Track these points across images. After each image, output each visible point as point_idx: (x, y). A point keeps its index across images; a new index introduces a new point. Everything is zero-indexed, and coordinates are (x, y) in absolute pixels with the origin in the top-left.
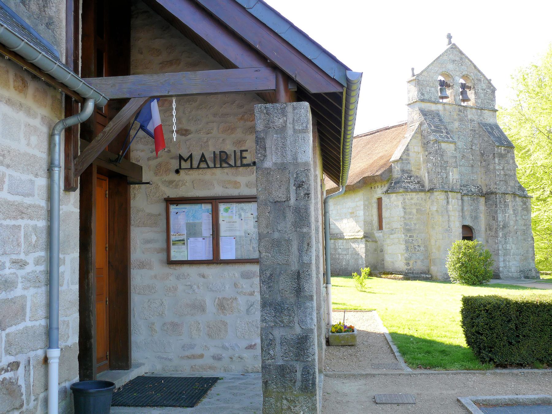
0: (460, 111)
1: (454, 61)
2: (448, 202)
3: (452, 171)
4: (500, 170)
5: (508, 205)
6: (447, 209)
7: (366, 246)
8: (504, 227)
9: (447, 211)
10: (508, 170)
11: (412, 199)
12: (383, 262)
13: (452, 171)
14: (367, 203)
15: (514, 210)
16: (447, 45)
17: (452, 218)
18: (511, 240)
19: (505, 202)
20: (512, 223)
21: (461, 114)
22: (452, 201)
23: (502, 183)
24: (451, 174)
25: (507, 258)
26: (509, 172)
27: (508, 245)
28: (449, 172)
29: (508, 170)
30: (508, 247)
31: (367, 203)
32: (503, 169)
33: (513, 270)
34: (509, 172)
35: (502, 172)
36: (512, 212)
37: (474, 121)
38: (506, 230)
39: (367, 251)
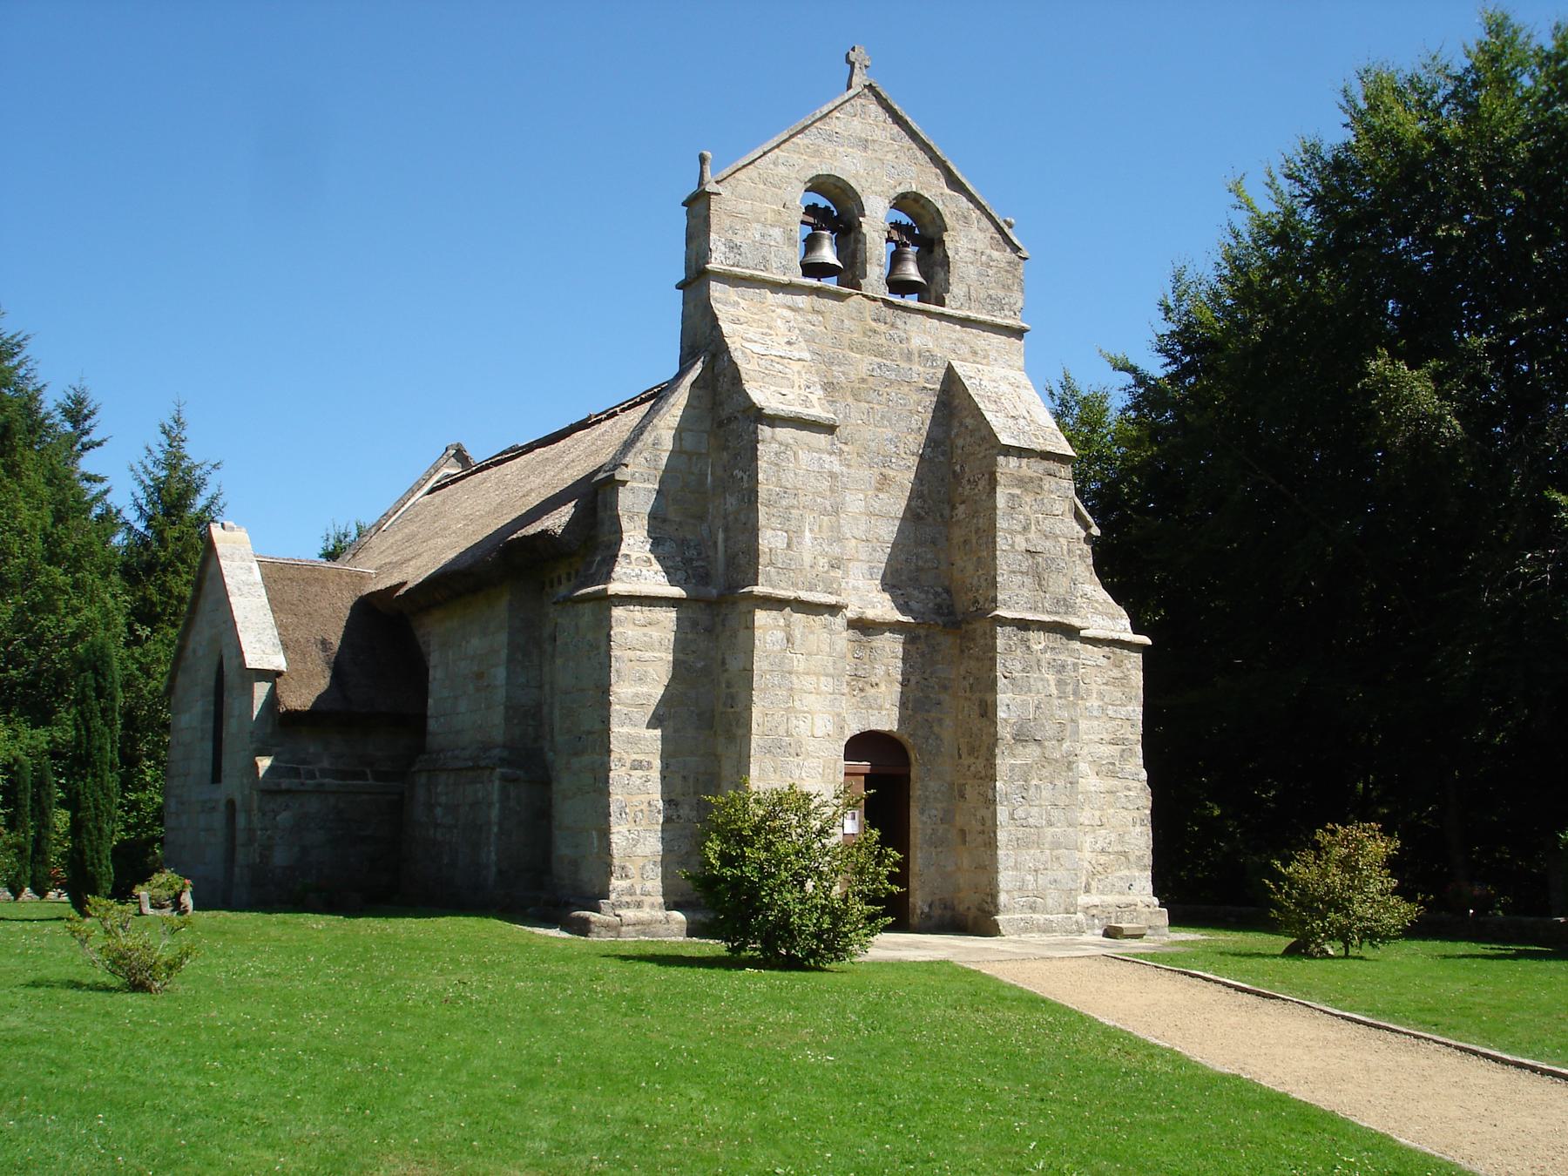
4: (1012, 532)
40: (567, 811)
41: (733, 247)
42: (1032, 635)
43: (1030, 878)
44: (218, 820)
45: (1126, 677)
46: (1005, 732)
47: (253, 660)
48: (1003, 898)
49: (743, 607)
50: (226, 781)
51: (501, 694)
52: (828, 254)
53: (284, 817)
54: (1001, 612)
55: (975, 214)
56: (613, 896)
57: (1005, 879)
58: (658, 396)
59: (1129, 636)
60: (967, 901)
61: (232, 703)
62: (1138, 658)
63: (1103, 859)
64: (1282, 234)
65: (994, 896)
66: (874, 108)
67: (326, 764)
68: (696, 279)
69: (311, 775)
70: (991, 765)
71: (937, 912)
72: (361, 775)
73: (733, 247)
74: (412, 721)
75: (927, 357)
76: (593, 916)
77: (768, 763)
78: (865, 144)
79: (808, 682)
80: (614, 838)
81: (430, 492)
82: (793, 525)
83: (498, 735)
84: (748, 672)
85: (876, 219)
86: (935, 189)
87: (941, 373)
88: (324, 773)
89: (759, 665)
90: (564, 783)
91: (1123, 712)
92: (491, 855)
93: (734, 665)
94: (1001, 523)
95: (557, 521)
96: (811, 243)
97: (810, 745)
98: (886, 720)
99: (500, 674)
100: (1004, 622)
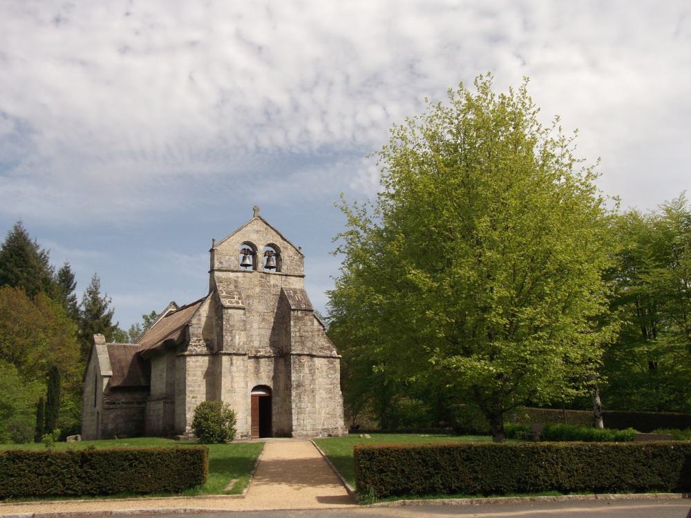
0: (262, 277)
1: (257, 232)
2: (232, 364)
3: (239, 334)
4: (296, 332)
5: (304, 365)
6: (230, 369)
7: (164, 407)
8: (298, 386)
9: (230, 373)
10: (304, 331)
11: (197, 361)
12: (473, 448)
13: (239, 334)
14: (170, 365)
15: (310, 370)
16: (75, 296)
17: (236, 379)
18: (306, 398)
19: (300, 362)
20: (307, 382)
21: (262, 279)
22: (236, 363)
23: (297, 344)
24: (237, 337)
25: (301, 417)
26: (306, 334)
27: (303, 404)
28: (235, 335)
29: (304, 331)
30: (303, 405)
31: (170, 365)
32: (299, 331)
33: (308, 428)
34: (306, 334)
35: (298, 334)
36: (307, 372)
37: (277, 286)
38: (302, 389)
39: (165, 412)
40: (178, 410)
41: (221, 263)
42: (316, 359)
43: (302, 422)
44: (95, 417)
45: (335, 367)
46: (294, 384)
47: (103, 373)
48: (294, 427)
49: (220, 356)
50: (97, 406)
51: (165, 380)
52: (248, 261)
53: (112, 416)
54: (293, 352)
55: (290, 247)
56: (187, 431)
57: (295, 423)
58: (202, 301)
59: (337, 356)
60: (286, 429)
61: (99, 385)
62: (338, 361)
63: (328, 416)
64: (543, 182)
65: (292, 426)
66: (260, 222)
67: (123, 400)
68: (212, 271)
69: (119, 404)
70: (291, 393)
71: (280, 432)
72: (133, 403)
73: (221, 263)
74: (147, 388)
75: (275, 286)
76: (181, 436)
77: (226, 395)
78: (257, 232)
79: (237, 374)
80: (187, 416)
81: (166, 316)
82: (233, 334)
83: (164, 391)
84: (221, 372)
85: (261, 249)
86: (279, 242)
87: (279, 290)
88: (123, 403)
89: (223, 370)
90: (177, 402)
91: (334, 376)
92: (161, 423)
93: (218, 371)
94: (292, 329)
95: (175, 337)
96: (244, 259)
97: (237, 390)
98: (266, 380)
99: (165, 375)
100: (293, 355)
